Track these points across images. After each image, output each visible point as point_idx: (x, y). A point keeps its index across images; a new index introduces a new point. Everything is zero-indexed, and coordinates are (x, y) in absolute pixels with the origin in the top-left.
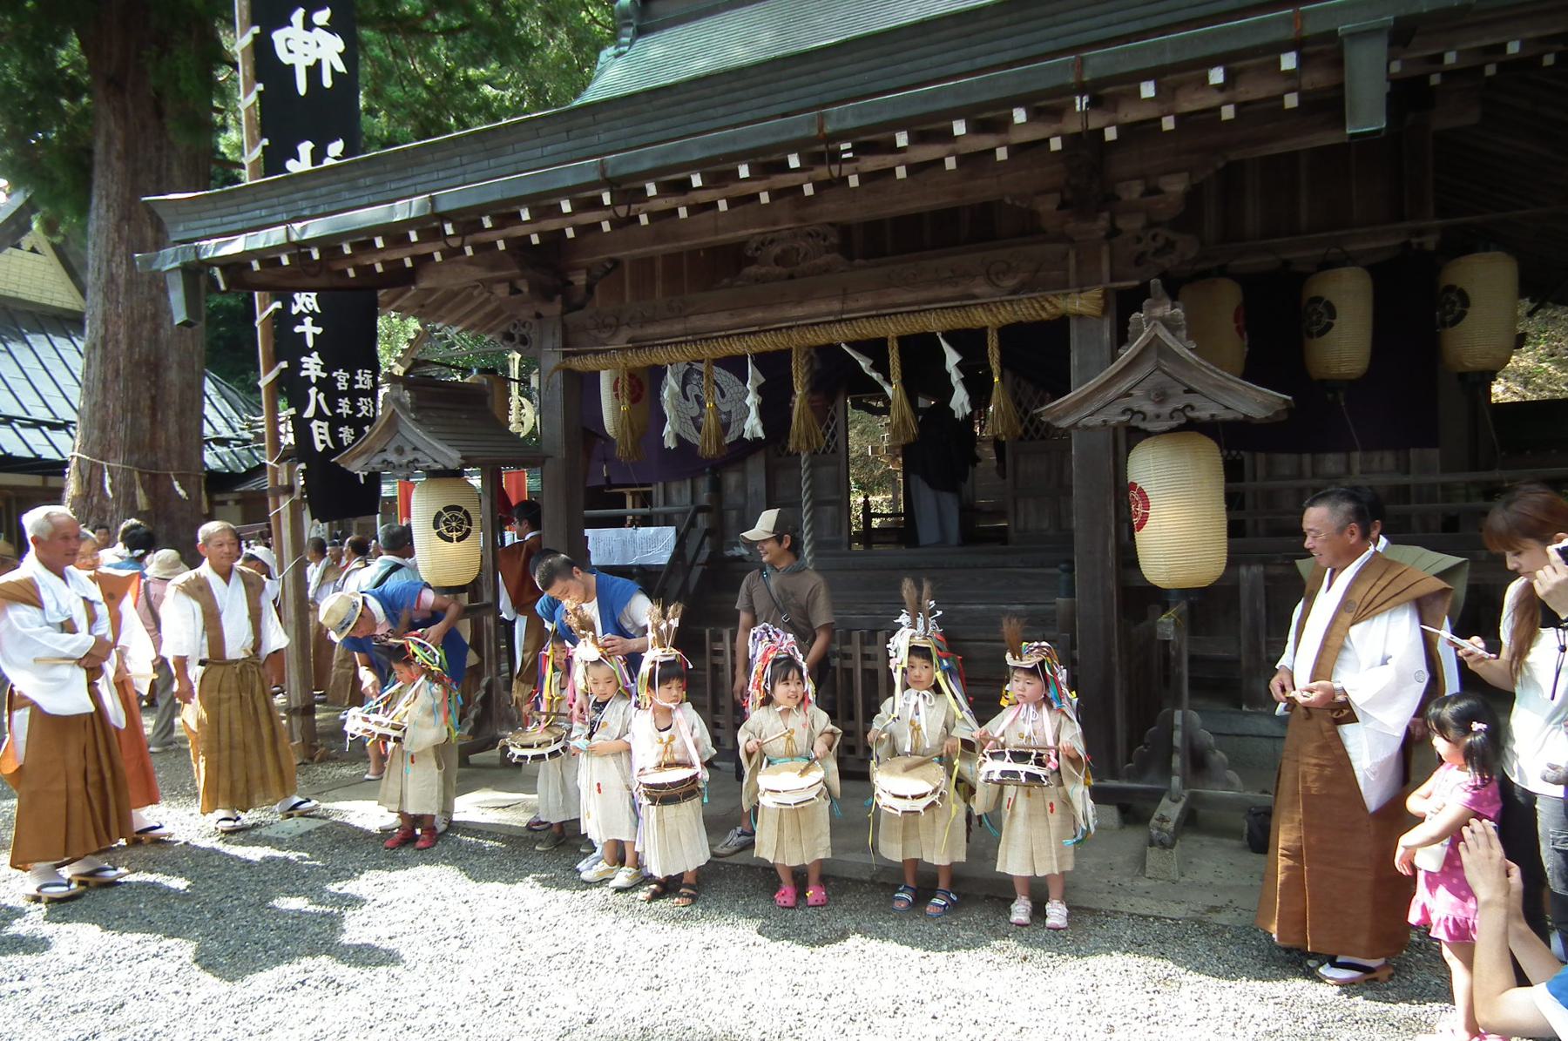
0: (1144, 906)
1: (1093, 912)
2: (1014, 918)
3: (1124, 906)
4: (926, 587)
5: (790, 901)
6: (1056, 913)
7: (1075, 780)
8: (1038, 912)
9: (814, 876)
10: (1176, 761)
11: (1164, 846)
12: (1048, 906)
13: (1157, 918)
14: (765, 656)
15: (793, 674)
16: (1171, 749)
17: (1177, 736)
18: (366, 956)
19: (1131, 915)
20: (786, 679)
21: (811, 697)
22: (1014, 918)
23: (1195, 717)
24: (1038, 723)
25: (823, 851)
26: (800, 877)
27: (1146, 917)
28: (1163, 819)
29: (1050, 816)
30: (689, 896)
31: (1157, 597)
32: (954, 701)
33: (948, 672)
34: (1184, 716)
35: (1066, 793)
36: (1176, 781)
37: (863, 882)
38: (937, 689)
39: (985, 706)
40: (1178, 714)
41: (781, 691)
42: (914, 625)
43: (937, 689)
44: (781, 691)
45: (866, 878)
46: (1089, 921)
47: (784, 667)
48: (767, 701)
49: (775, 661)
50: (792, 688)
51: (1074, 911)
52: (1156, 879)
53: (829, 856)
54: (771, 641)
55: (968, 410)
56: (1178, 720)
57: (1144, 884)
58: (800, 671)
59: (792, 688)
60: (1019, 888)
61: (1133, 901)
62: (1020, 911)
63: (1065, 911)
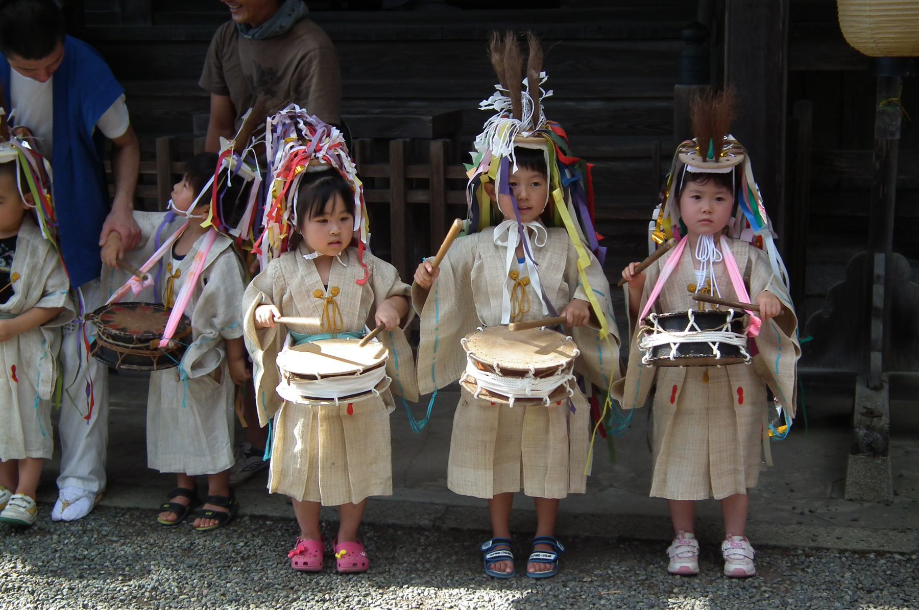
0: (857, 538)
1: (785, 551)
2: (676, 566)
3: (826, 539)
4: (533, 45)
5: (312, 559)
6: (738, 555)
7: (779, 346)
8: (711, 555)
9: (347, 527)
10: (877, 329)
11: (875, 451)
12: (726, 545)
13: (880, 554)
14: (288, 168)
15: (336, 203)
16: (868, 310)
17: (878, 291)
18: (864, 408)
19: (842, 552)
20: (321, 212)
21: (365, 239)
22: (676, 566)
23: (903, 262)
24: (721, 263)
25: (379, 484)
26: (328, 524)
27: (863, 554)
28: (871, 413)
29: (738, 408)
30: (216, 515)
31: (866, 72)
32: (574, 244)
33: (572, 190)
34: (888, 261)
35: (763, 363)
36: (876, 358)
37: (420, 529)
38: (550, 219)
39: (622, 245)
40: (879, 260)
41: (313, 232)
42: (515, 112)
43: (550, 219)
44: (313, 232)
45: (425, 522)
46: (784, 564)
47: (319, 189)
48: (293, 243)
49: (307, 178)
50: (334, 228)
51: (763, 551)
52: (862, 500)
53: (389, 492)
54: (300, 137)
55: (278, 389)
56: (879, 269)
57: (845, 508)
58: (348, 194)
59: (333, 228)
60: (681, 520)
61: (838, 531)
62: (683, 555)
63: (750, 551)
